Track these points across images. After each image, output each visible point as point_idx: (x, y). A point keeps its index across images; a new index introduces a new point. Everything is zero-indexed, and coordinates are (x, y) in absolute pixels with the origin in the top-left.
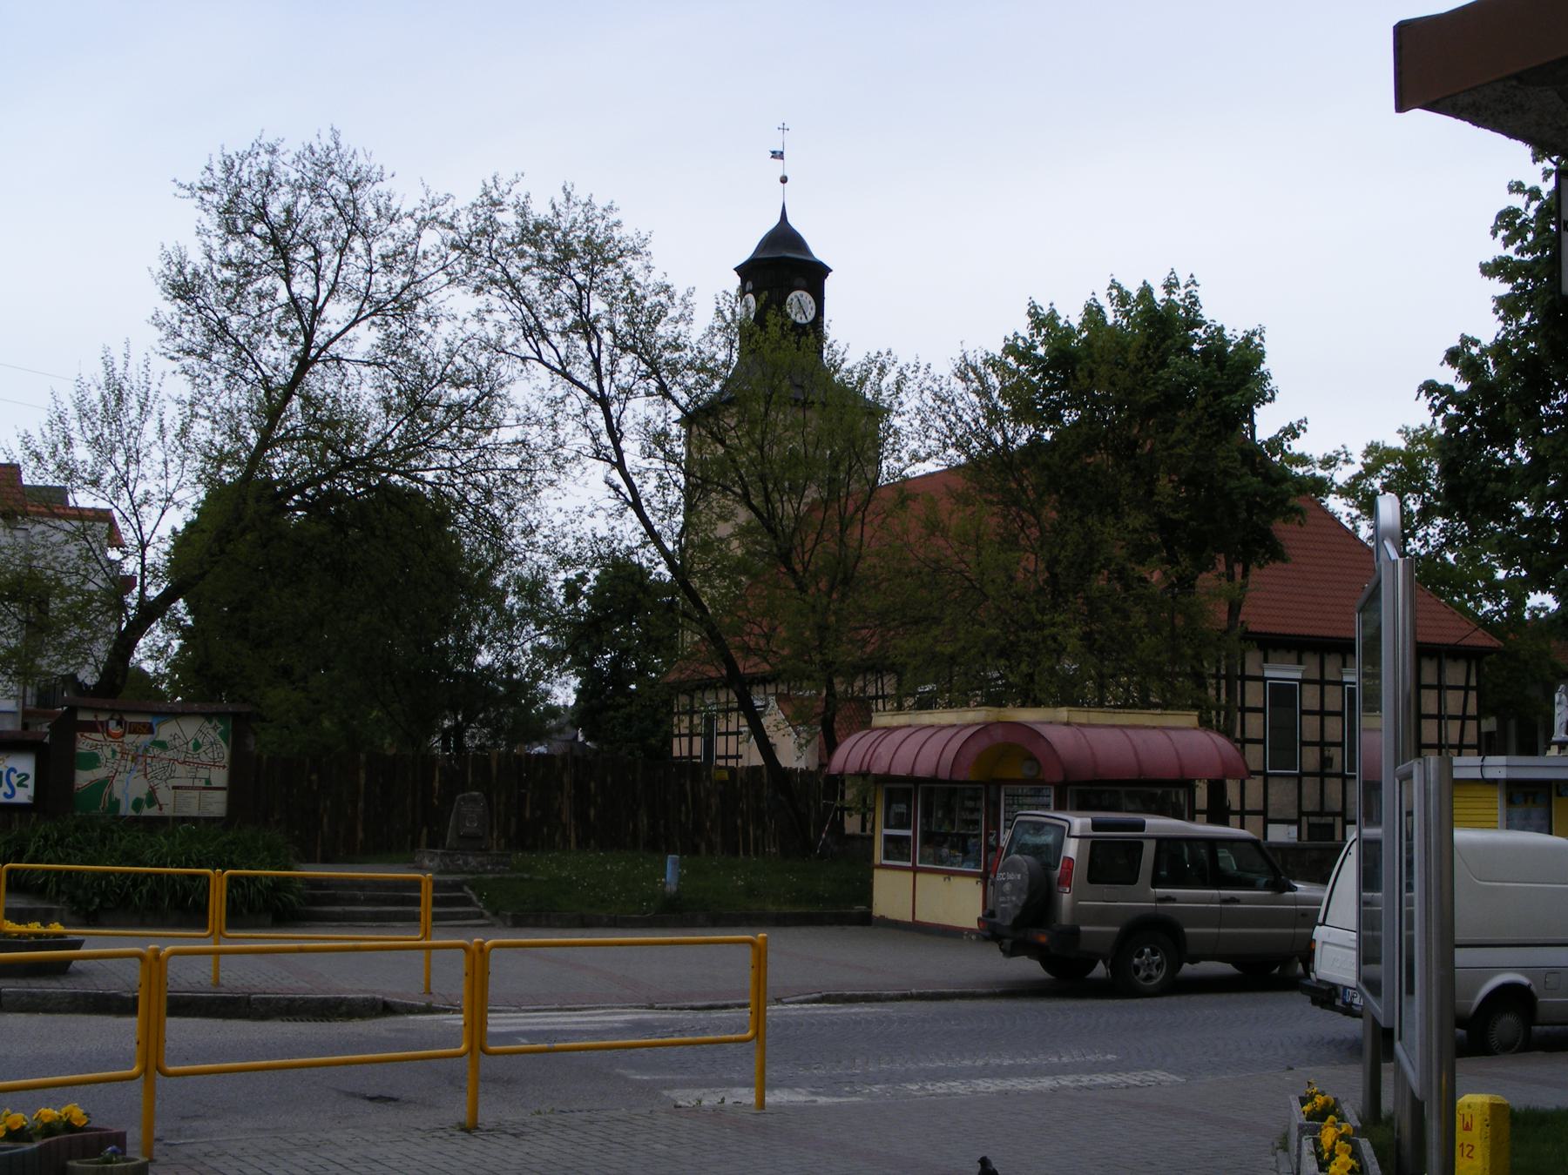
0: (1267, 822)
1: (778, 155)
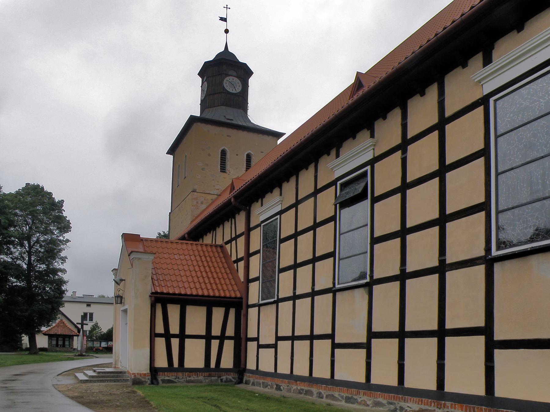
0: (260, 346)
1: (224, 19)
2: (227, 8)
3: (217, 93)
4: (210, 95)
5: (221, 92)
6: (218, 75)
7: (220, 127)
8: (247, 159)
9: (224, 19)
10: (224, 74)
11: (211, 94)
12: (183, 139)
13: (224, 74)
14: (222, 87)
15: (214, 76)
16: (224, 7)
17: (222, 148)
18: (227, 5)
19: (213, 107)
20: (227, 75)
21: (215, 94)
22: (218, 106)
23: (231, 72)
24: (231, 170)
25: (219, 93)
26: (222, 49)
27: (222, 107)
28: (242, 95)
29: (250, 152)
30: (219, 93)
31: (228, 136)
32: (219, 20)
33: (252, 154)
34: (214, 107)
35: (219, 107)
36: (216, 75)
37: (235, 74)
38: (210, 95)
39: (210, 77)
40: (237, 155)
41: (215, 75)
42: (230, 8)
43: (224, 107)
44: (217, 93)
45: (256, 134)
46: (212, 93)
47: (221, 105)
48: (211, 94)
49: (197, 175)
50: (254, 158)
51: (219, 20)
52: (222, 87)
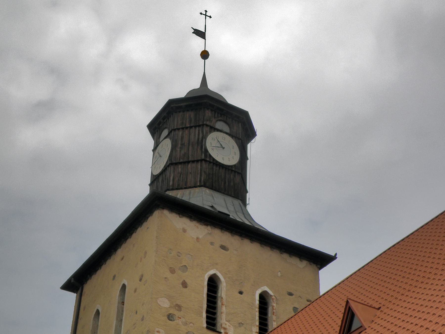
2: (206, 15)
3: (193, 162)
4: (176, 164)
5: (201, 160)
6: (195, 127)
7: (207, 225)
8: (207, 317)
9: (201, 34)
10: (207, 125)
11: (180, 163)
12: (115, 250)
13: (207, 125)
14: (203, 150)
15: (187, 128)
16: (201, 14)
17: (212, 272)
18: (206, 11)
19: (182, 189)
20: (214, 129)
21: (188, 162)
22: (195, 187)
23: (220, 125)
24: (228, 327)
25: (197, 161)
26: (197, 85)
27: (204, 189)
28: (240, 172)
29: (266, 288)
30: (197, 161)
31: (223, 247)
32: (193, 33)
33: (271, 295)
34: (186, 188)
35: (197, 190)
36: (191, 127)
37: (226, 128)
38: (176, 164)
39: (178, 129)
40: (241, 293)
41: (188, 125)
42: (210, 17)
43: (208, 191)
44: (193, 162)
45: (278, 251)
46: (181, 161)
47: (200, 186)
48: (180, 163)
49: (157, 329)
50: (275, 305)
51: (193, 33)
52: (203, 150)
